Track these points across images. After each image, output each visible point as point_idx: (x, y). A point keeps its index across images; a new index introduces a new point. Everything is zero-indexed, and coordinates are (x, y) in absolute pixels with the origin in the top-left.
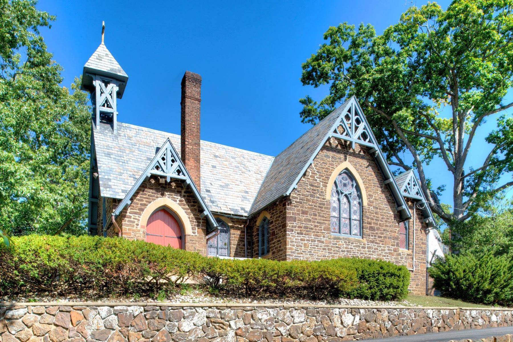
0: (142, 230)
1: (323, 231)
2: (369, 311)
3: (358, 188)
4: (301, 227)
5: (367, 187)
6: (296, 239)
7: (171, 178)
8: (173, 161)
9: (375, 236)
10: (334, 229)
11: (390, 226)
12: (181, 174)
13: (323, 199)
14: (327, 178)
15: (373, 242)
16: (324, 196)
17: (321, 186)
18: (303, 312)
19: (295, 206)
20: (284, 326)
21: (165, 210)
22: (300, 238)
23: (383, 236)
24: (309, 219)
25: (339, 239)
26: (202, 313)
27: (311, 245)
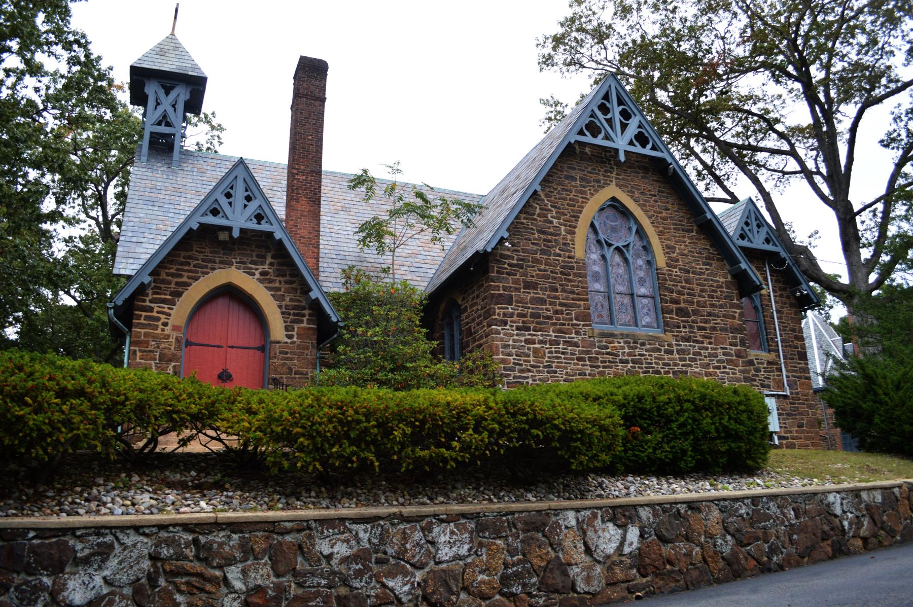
0: (175, 334)
1: (575, 322)
2: (665, 511)
3: (641, 233)
4: (525, 316)
5: (661, 232)
6: (514, 341)
7: (242, 231)
8: (248, 198)
9: (691, 327)
10: (600, 316)
11: (721, 306)
12: (263, 222)
13: (569, 257)
14: (574, 216)
15: (687, 340)
16: (571, 251)
17: (563, 233)
18: (462, 528)
19: (508, 274)
20: (405, 573)
21: (231, 292)
22: (523, 339)
23: (707, 325)
24: (542, 298)
25: (612, 335)
26: (135, 545)
27: (551, 352)
